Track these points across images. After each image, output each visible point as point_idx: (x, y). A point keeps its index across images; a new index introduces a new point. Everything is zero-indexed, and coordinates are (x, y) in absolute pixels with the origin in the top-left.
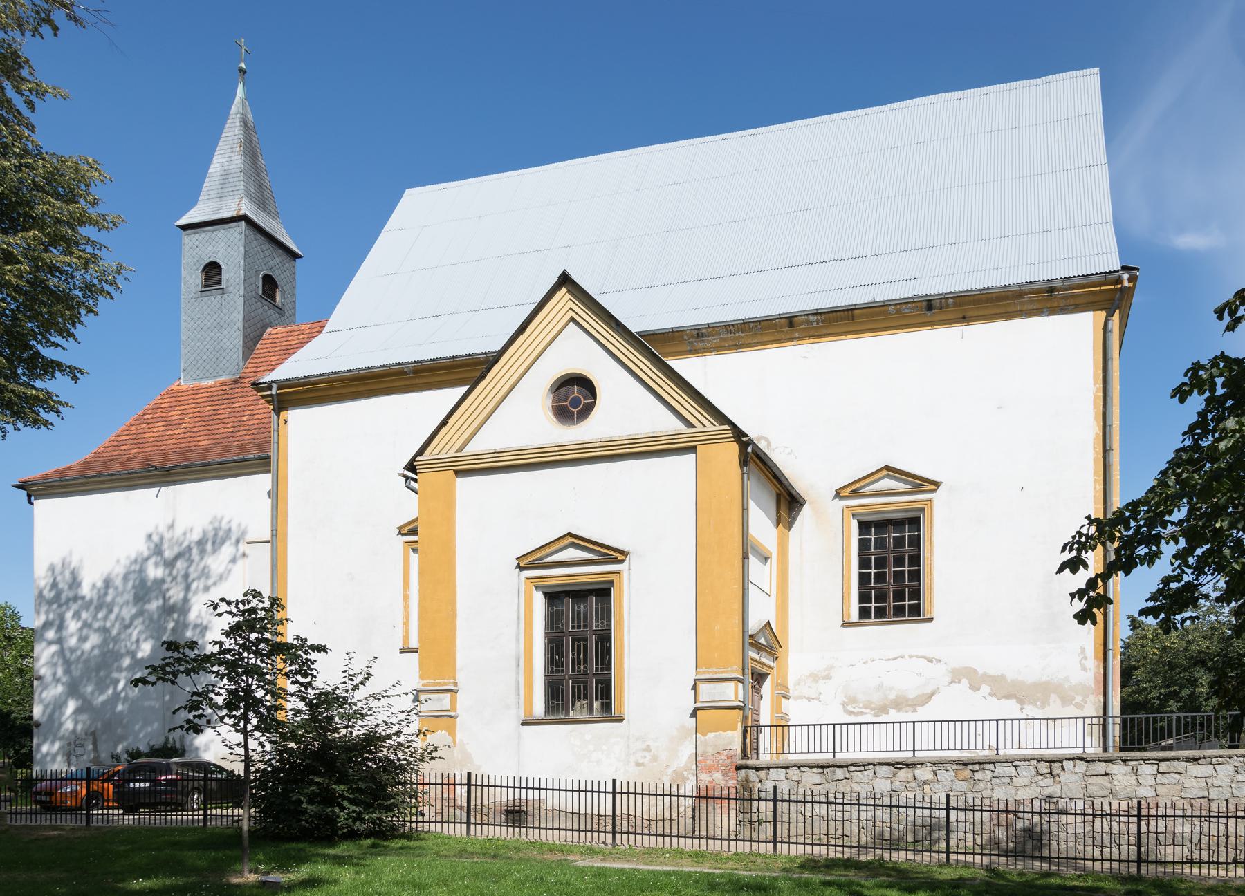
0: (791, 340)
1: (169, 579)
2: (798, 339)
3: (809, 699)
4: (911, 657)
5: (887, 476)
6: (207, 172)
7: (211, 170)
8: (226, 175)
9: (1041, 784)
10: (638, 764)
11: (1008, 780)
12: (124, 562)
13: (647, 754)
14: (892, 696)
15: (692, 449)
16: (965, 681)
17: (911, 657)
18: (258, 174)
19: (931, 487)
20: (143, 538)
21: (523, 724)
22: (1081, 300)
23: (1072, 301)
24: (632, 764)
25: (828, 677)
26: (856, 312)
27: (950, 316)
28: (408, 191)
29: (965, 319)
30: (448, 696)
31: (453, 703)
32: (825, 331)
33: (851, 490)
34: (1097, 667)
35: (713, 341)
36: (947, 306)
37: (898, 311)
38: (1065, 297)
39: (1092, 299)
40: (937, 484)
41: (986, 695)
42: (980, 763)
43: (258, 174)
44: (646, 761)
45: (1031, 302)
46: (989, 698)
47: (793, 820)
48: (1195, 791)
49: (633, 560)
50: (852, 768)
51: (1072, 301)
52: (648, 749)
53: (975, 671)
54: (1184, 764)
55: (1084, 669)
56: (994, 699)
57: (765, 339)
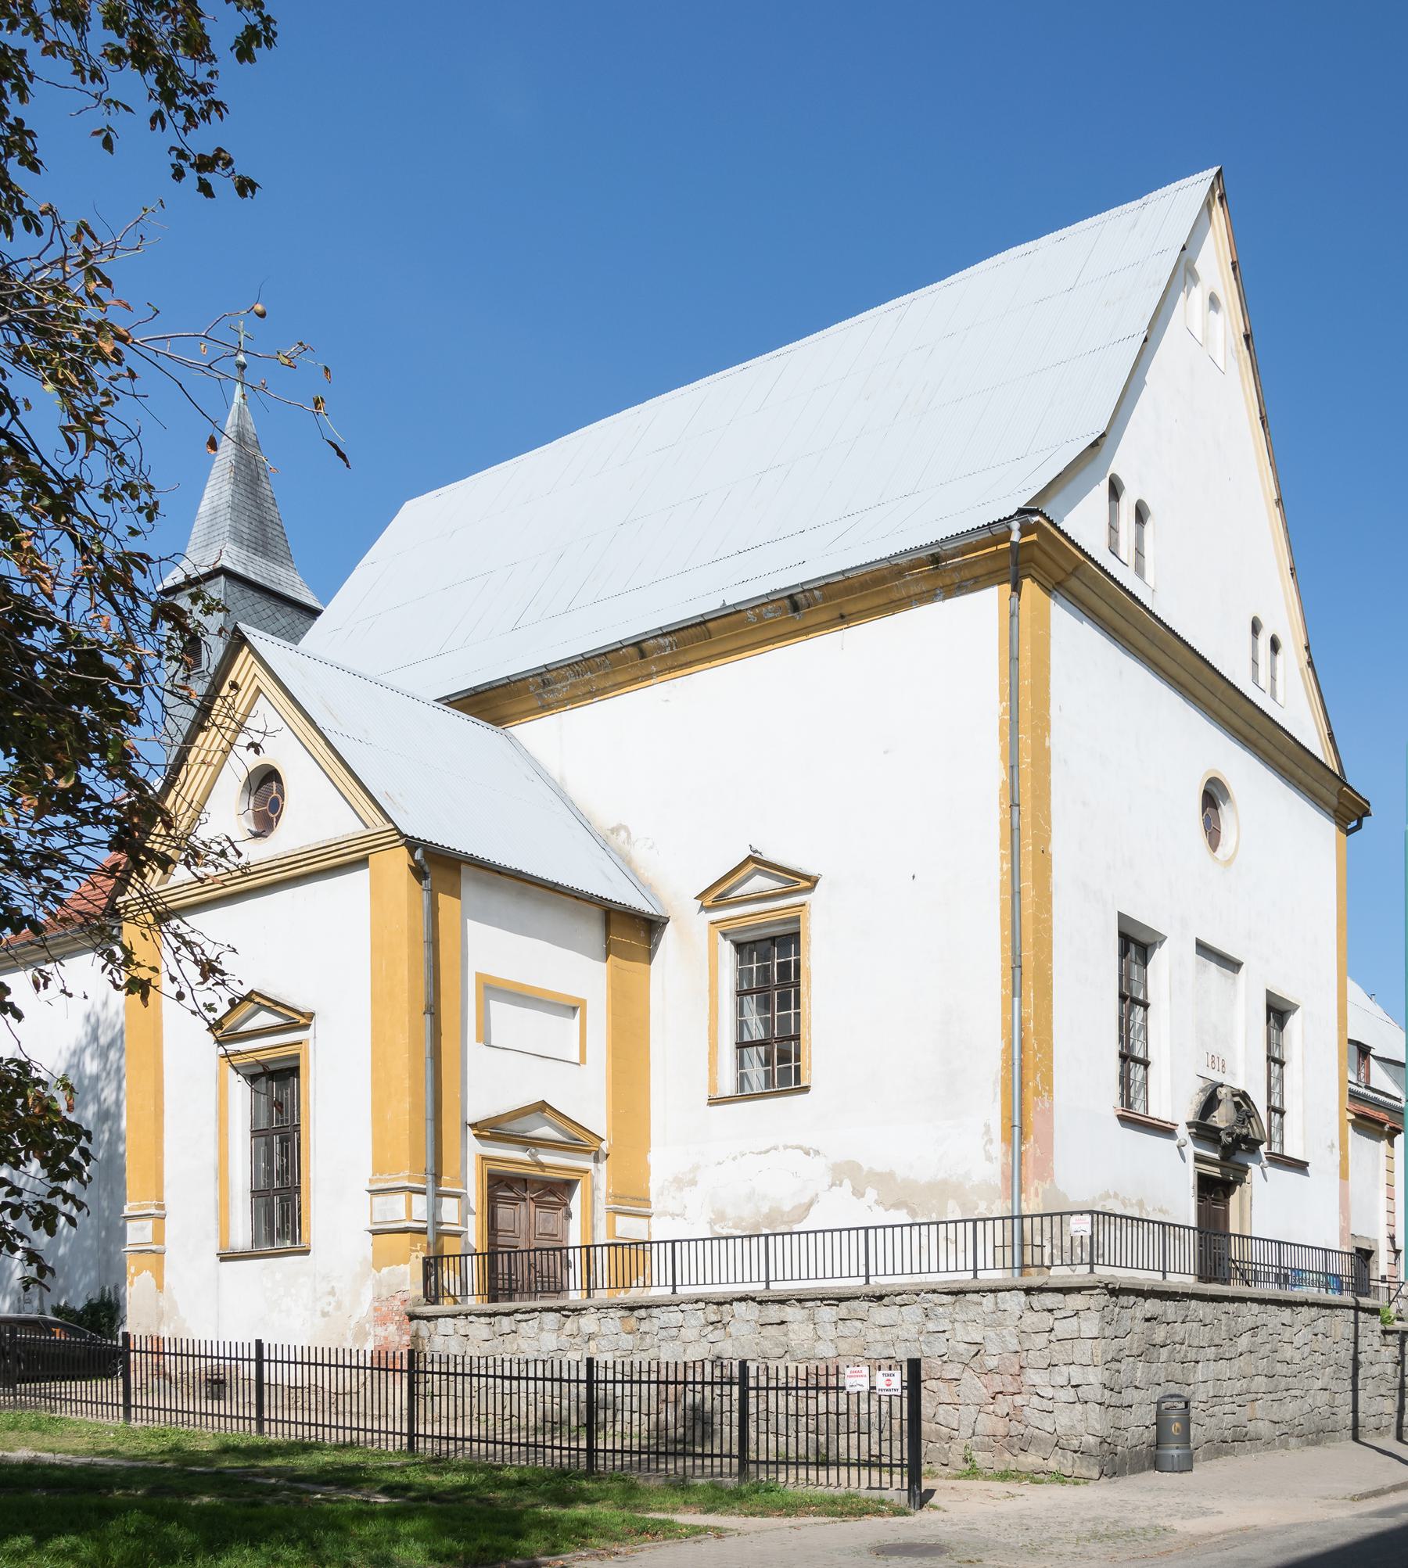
0: (649, 676)
1: (104, 1075)
2: (659, 673)
3: (673, 1216)
4: (786, 1147)
5: (757, 872)
6: (196, 514)
7: (201, 510)
8: (215, 512)
9: (711, 1338)
10: (325, 1314)
11: (674, 1332)
12: (66, 1055)
13: (331, 1299)
14: (765, 1209)
15: (363, 862)
16: (847, 1183)
17: (786, 1147)
18: (259, 506)
19: (804, 884)
20: (81, 1019)
21: (222, 1260)
22: (978, 571)
23: (966, 574)
24: (319, 1313)
25: (693, 1183)
26: (710, 625)
27: (823, 617)
28: (409, 506)
29: (843, 619)
30: (149, 1224)
31: (159, 1236)
32: (683, 659)
33: (716, 896)
34: (1005, 1154)
35: (562, 689)
36: (816, 602)
37: (760, 618)
38: (957, 568)
39: (992, 565)
40: (813, 881)
41: (872, 1203)
42: (647, 1307)
43: (259, 506)
44: (330, 1309)
45: (917, 581)
46: (875, 1208)
47: (653, 1409)
48: (879, 1347)
49: (317, 1023)
50: (519, 1317)
51: (966, 574)
52: (332, 1293)
53: (860, 1167)
54: (866, 1304)
55: (989, 1159)
56: (881, 1209)
57: (620, 679)
